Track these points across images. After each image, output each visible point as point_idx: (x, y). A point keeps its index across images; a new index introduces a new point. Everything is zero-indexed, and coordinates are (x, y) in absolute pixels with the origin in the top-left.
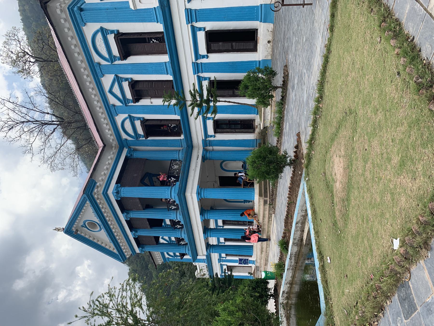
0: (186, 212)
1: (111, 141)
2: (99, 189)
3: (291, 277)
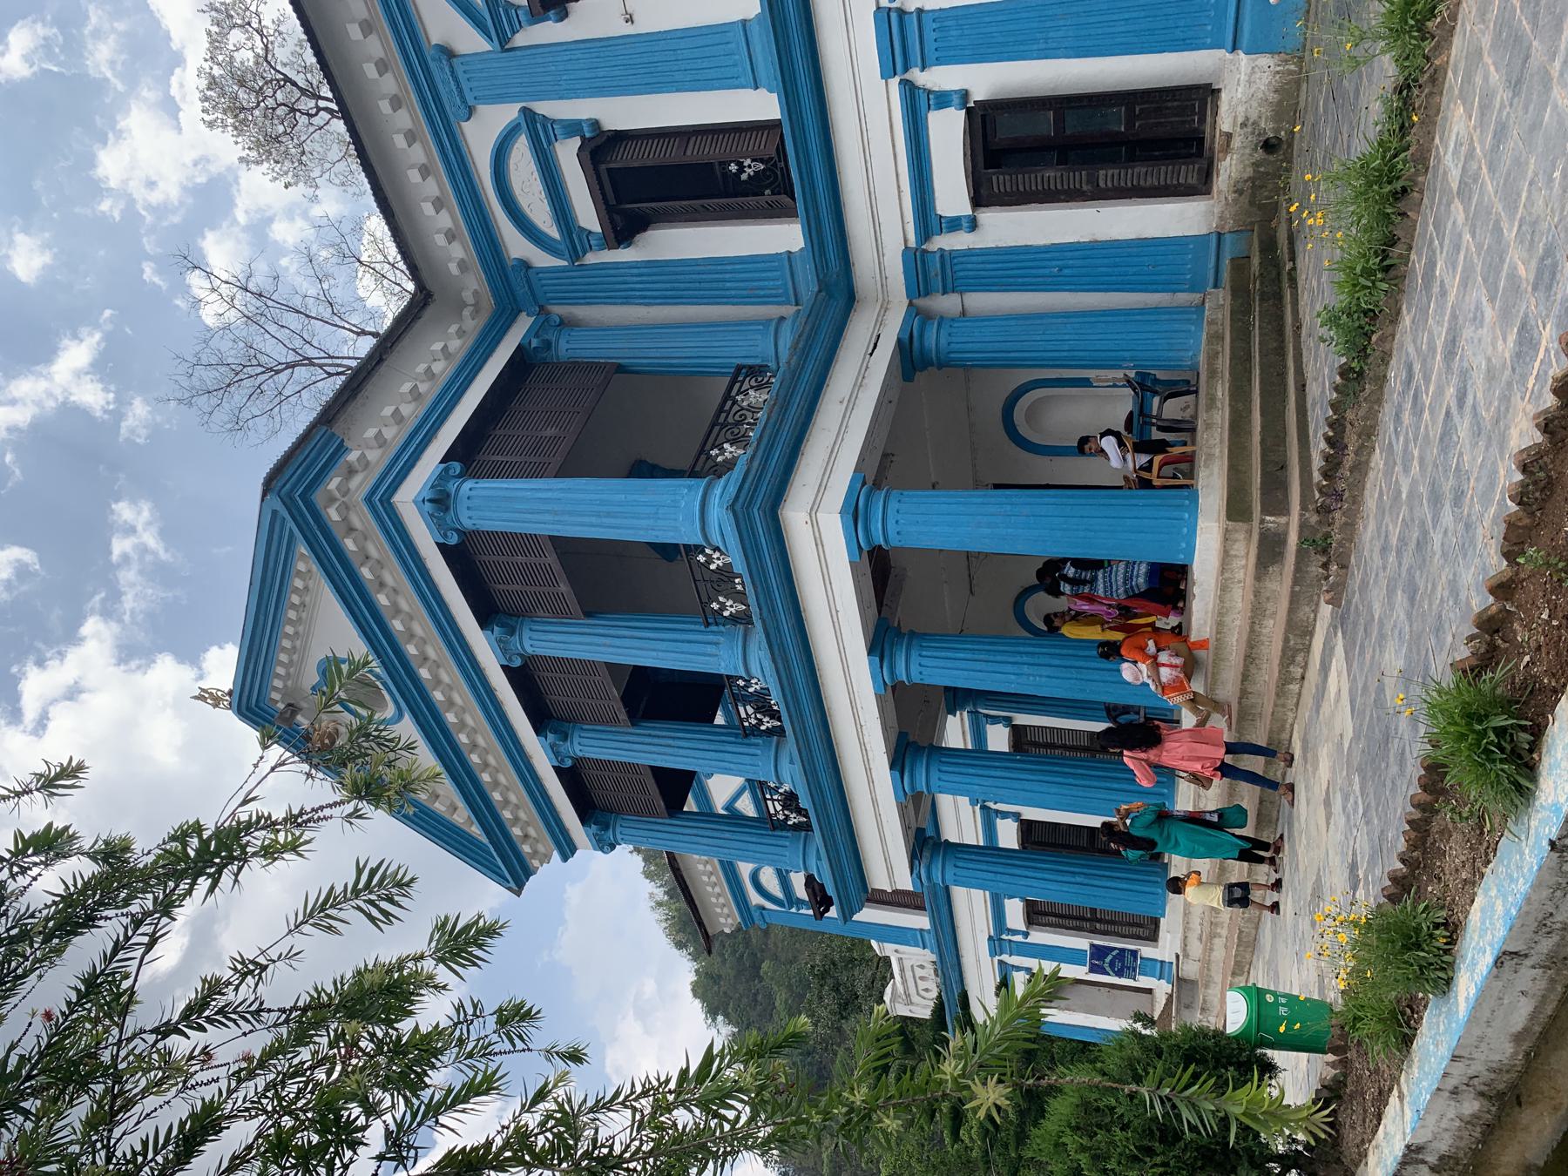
0: (786, 625)
1: (453, 268)
2: (354, 483)
3: (1518, 1038)
